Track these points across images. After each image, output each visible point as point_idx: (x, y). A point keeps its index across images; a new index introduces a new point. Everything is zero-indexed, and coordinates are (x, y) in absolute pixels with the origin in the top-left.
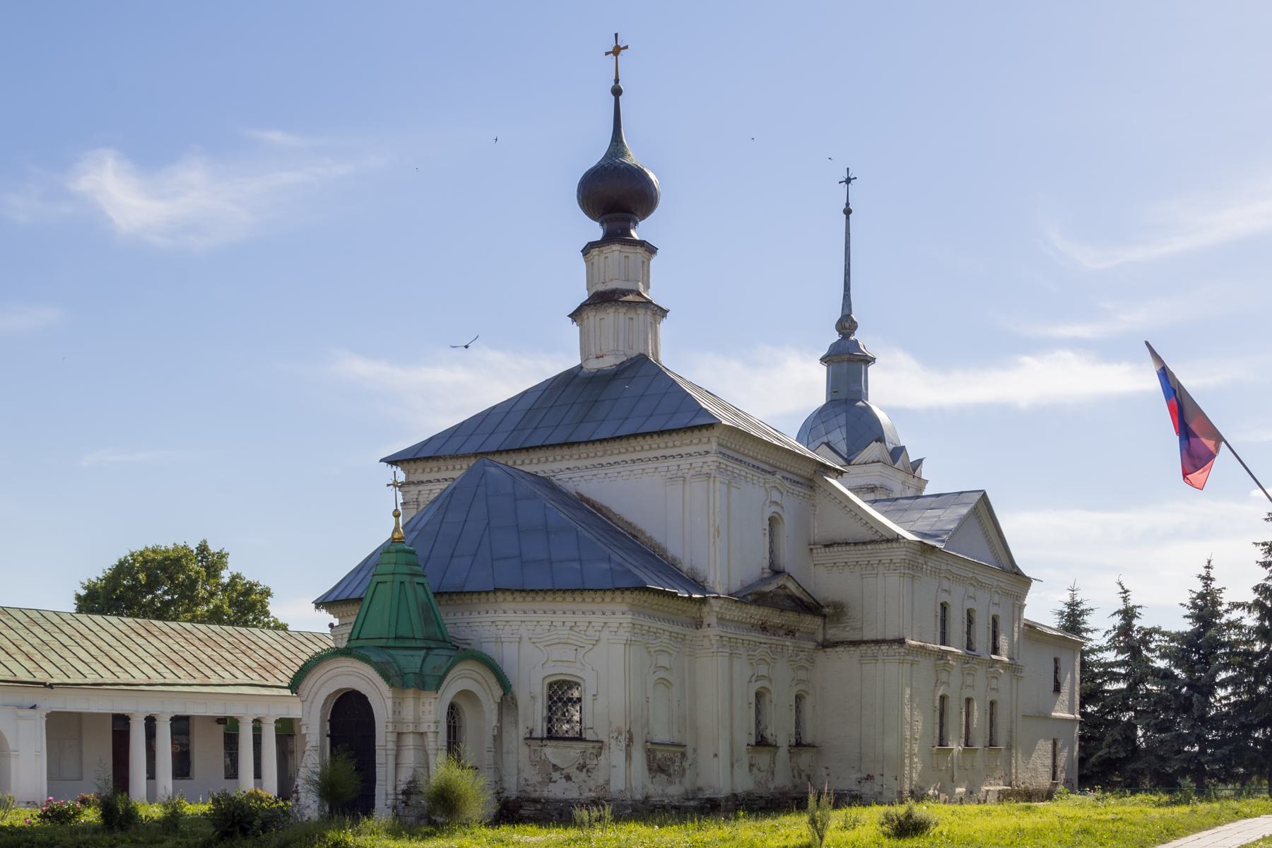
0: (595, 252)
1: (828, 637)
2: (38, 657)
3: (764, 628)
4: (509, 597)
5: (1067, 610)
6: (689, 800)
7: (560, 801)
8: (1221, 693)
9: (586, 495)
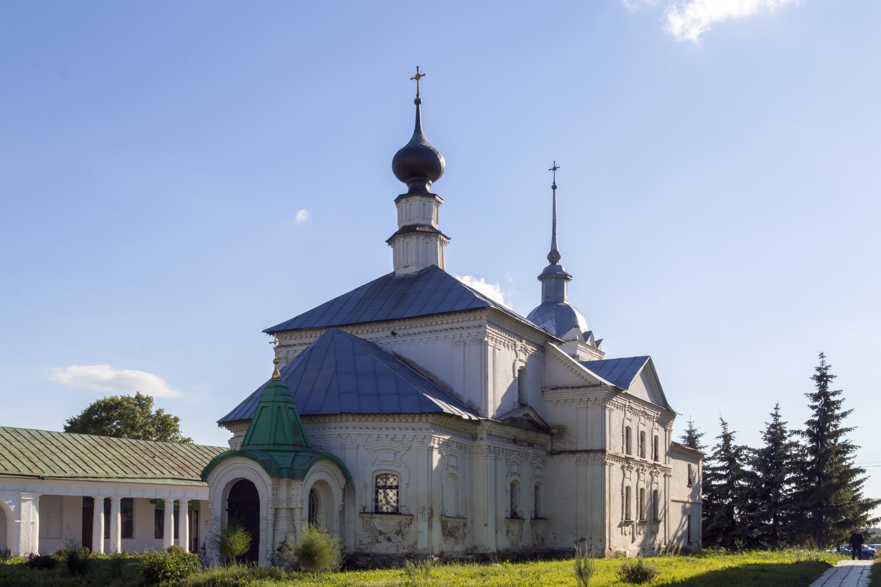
0: (404, 201)
1: (554, 448)
2: (35, 460)
3: (515, 441)
4: (350, 418)
5: (687, 435)
6: (469, 554)
7: (384, 555)
8: (787, 487)
9: (399, 354)
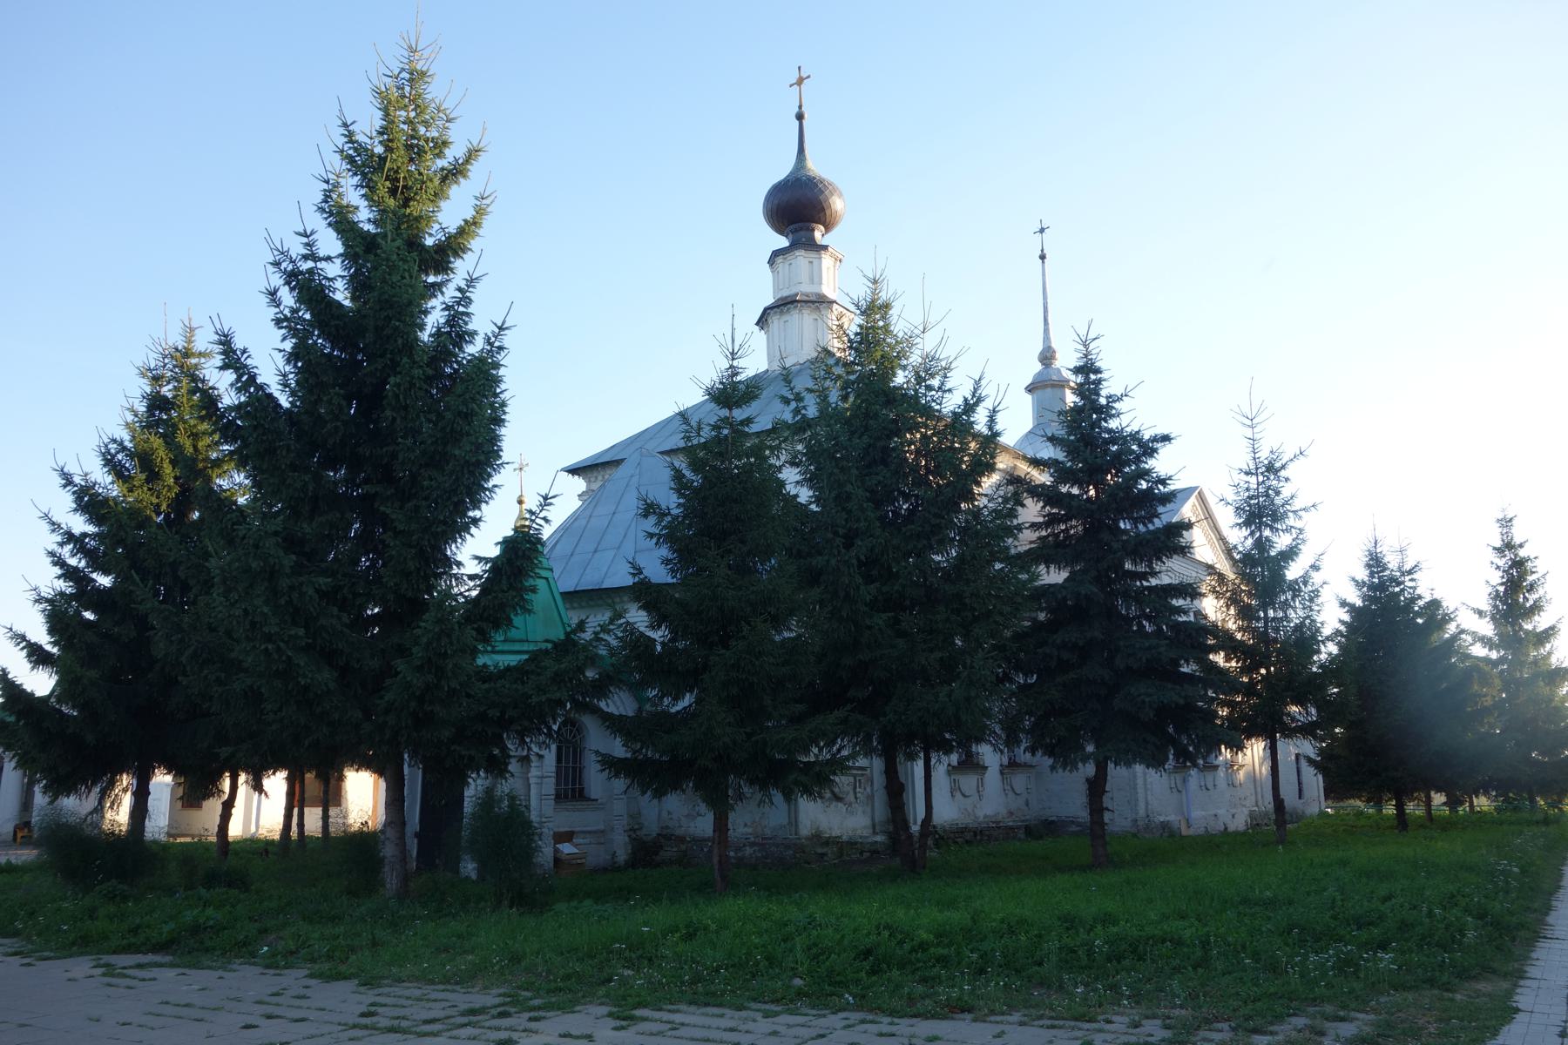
0: (779, 260)
